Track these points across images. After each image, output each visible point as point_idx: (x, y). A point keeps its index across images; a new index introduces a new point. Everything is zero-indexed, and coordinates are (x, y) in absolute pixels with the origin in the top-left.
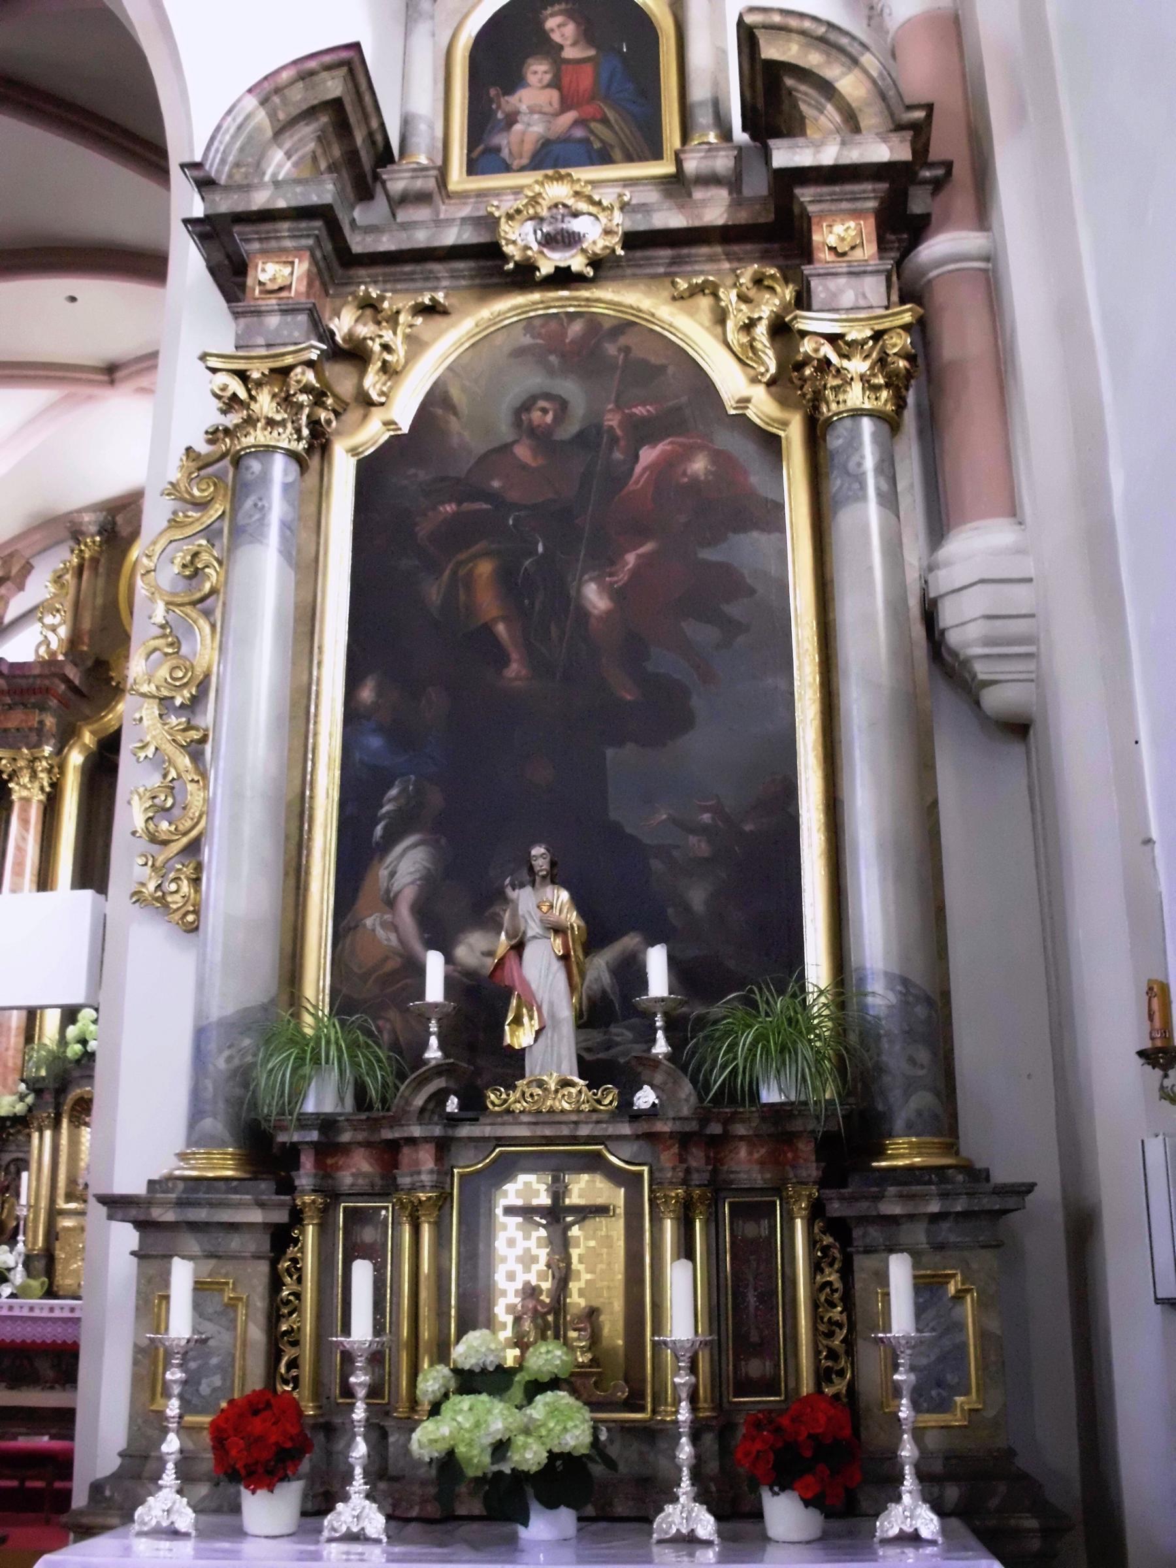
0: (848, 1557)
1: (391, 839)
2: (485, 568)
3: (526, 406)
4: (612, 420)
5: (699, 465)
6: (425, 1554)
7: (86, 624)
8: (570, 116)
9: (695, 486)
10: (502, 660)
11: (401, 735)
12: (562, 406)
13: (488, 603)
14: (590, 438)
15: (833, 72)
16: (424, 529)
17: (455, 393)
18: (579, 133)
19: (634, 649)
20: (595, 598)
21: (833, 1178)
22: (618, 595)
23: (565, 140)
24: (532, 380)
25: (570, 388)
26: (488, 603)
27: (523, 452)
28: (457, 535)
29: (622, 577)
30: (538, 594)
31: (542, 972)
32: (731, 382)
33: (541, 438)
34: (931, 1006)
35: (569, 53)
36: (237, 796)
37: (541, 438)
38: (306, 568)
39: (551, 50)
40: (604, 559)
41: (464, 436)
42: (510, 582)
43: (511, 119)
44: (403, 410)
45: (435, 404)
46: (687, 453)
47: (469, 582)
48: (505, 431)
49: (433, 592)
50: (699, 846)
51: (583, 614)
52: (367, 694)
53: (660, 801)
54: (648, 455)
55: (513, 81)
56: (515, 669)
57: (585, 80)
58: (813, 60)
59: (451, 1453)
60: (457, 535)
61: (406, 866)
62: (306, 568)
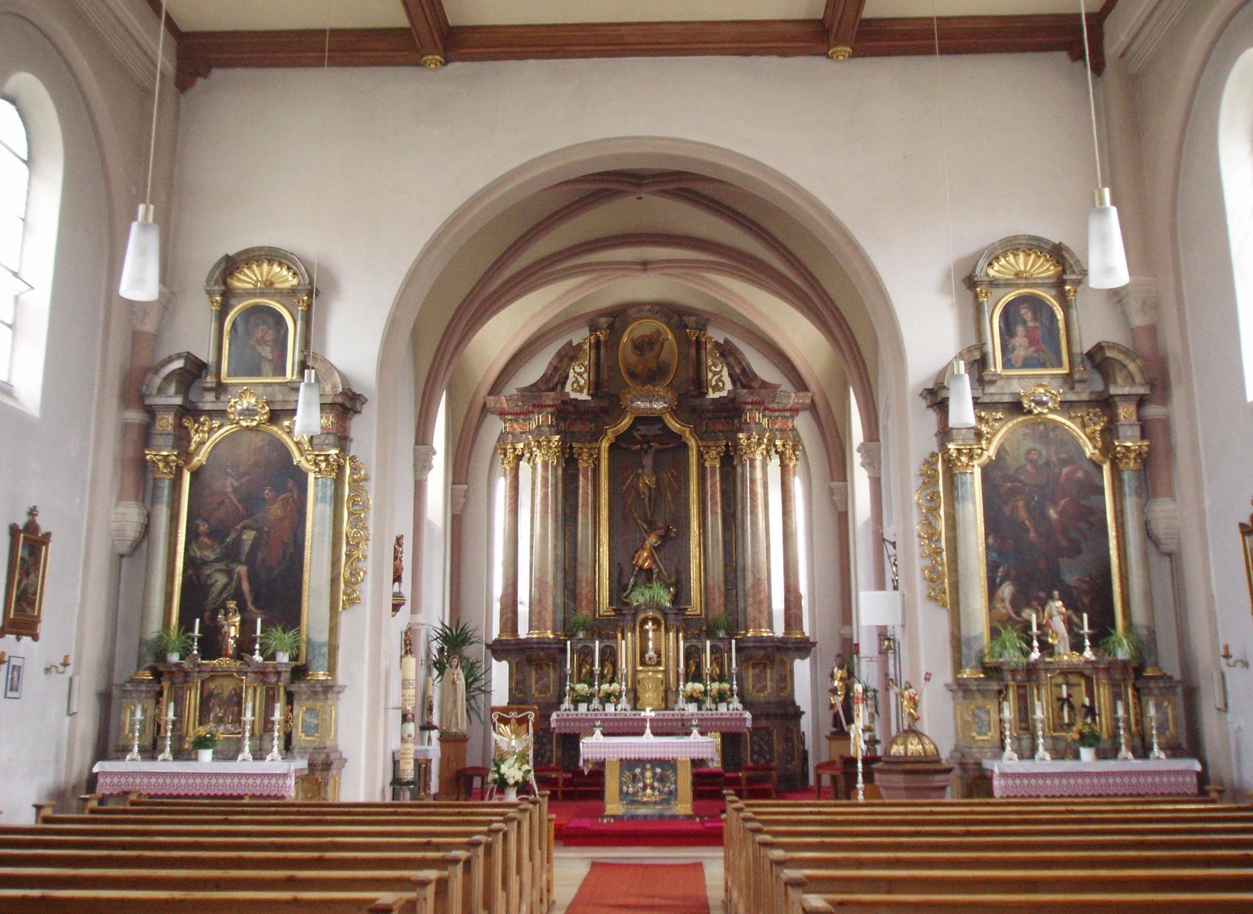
0: (791, 297)
1: (1000, 585)
2: (1021, 504)
3: (1029, 452)
4: (1054, 459)
5: (1080, 474)
6: (711, 262)
8: (1033, 348)
10: (1027, 531)
11: (1000, 552)
12: (1040, 454)
13: (1023, 514)
15: (1127, 362)
17: (1007, 447)
18: (1036, 355)
20: (1053, 514)
21: (1137, 678)
22: (1060, 513)
23: (1031, 358)
24: (1030, 444)
26: (1023, 514)
27: (1029, 468)
28: (1013, 492)
29: (1060, 508)
30: (1038, 513)
31: (1059, 625)
32: (1089, 450)
34: (1152, 632)
36: (905, 500)
39: (1024, 323)
40: (1054, 503)
41: (1011, 463)
42: (1029, 510)
43: (1014, 349)
44: (991, 452)
45: (1001, 451)
47: (1017, 507)
48: (1023, 461)
49: (1007, 510)
51: (1049, 520)
52: (991, 540)
54: (1065, 470)
56: (1032, 534)
58: (1121, 357)
60: (1013, 492)
62: (174, 519)
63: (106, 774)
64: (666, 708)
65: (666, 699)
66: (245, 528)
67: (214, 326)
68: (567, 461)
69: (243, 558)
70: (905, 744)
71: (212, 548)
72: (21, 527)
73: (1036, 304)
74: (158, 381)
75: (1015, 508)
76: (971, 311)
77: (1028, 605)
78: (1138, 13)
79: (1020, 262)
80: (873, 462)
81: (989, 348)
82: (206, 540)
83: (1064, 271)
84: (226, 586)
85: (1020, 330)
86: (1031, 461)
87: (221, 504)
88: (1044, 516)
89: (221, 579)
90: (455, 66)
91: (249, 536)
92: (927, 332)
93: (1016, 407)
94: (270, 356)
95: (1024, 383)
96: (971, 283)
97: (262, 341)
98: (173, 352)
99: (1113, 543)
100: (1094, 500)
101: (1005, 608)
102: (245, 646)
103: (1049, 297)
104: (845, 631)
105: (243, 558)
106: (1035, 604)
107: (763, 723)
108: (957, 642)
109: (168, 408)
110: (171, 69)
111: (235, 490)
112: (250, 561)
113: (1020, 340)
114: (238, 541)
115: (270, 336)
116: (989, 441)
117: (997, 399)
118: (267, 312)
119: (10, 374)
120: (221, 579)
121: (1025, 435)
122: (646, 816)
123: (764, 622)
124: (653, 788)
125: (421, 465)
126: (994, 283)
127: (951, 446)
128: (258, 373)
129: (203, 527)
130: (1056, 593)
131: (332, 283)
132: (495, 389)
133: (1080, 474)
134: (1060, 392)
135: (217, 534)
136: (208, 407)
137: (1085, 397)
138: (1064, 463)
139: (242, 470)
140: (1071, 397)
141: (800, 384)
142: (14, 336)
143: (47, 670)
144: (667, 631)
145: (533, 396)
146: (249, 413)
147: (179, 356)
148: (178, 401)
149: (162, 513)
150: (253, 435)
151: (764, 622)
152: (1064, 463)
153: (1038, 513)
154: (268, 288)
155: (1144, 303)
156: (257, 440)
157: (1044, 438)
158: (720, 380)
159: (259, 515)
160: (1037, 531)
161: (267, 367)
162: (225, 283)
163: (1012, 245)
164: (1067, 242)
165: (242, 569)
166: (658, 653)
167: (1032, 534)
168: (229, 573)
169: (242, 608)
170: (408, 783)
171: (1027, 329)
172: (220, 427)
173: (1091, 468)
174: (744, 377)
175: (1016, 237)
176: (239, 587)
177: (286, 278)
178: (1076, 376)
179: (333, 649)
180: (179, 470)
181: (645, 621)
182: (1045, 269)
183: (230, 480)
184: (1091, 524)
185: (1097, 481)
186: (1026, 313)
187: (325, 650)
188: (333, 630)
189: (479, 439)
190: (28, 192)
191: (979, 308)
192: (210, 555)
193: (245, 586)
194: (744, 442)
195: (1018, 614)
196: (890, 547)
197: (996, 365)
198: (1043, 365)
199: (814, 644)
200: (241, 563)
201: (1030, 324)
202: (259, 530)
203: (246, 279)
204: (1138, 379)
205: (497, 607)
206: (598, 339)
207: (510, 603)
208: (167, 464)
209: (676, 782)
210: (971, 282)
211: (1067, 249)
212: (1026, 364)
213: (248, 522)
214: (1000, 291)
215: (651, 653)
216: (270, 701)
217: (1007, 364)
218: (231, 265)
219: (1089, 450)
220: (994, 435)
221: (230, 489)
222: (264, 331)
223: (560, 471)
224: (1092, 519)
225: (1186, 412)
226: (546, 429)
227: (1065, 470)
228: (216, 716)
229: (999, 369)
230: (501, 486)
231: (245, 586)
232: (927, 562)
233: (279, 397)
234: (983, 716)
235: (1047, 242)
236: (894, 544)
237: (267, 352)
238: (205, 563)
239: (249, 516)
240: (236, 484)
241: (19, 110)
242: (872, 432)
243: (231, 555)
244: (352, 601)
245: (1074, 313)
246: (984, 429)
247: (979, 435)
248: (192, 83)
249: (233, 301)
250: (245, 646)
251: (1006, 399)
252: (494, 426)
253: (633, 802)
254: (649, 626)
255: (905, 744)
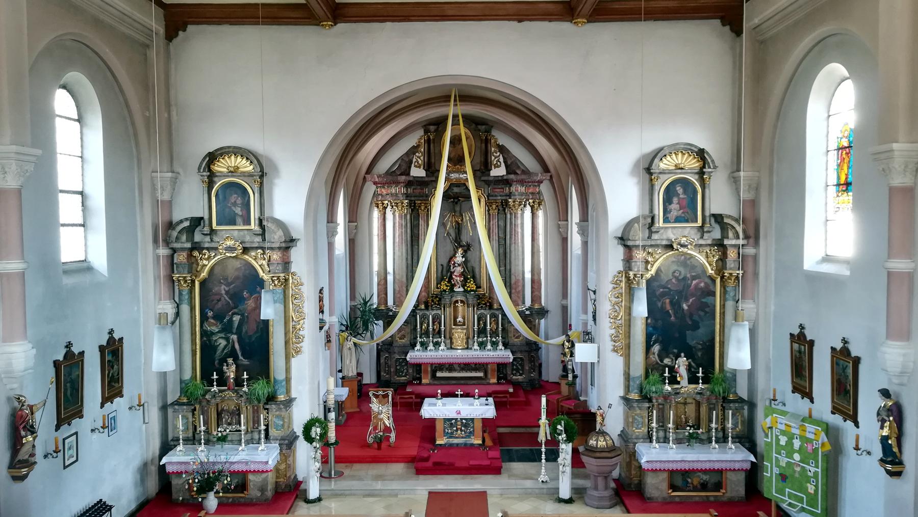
1: (654, 344)
2: (668, 301)
4: (688, 276)
5: (702, 285)
7: (397, 289)
9: (701, 288)
11: (654, 328)
13: (668, 307)
14: (685, 279)
15: (736, 225)
16: (658, 293)
19: (691, 315)
20: (685, 307)
22: (689, 306)
24: (675, 267)
25: (682, 269)
26: (668, 307)
27: (674, 281)
28: (663, 295)
30: (676, 305)
33: (676, 278)
35: (681, 196)
37: (676, 278)
38: (192, 309)
40: (687, 300)
44: (653, 272)
45: (658, 271)
46: (701, 282)
49: (659, 304)
50: (700, 347)
53: (694, 339)
54: (694, 282)
55: (671, 203)
56: (673, 318)
57: (685, 203)
58: (733, 223)
59: (547, 311)
61: (656, 348)
62: (192, 309)
63: (170, 463)
64: (467, 348)
65: (467, 343)
66: (233, 314)
67: (206, 196)
68: (412, 210)
69: (234, 331)
70: (597, 440)
71: (215, 325)
72: (105, 344)
73: (685, 183)
74: (175, 234)
75: (664, 303)
76: (647, 187)
77: (667, 357)
78: (768, 12)
79: (679, 159)
80: (583, 232)
81: (656, 212)
82: (212, 321)
83: (704, 167)
84: (225, 347)
85: (675, 200)
86: (675, 277)
87: (219, 300)
88: (680, 307)
89: (223, 343)
90: (341, 26)
91: (236, 319)
92: (622, 199)
93: (670, 247)
94: (240, 213)
95: (675, 231)
96: (647, 169)
97: (235, 204)
98: (182, 218)
99: (718, 326)
100: (708, 300)
101: (654, 358)
102: (239, 382)
103: (694, 179)
104: (564, 302)
105: (234, 331)
106: (671, 356)
107: (519, 355)
108: (627, 377)
109: (183, 249)
110: (162, 31)
111: (227, 293)
112: (239, 332)
113: (674, 206)
114: (231, 321)
115: (239, 201)
116: (652, 265)
117: (659, 242)
118: (236, 190)
119: (86, 257)
120: (223, 343)
121: (673, 262)
122: (457, 444)
123: (520, 303)
124: (461, 430)
125: (332, 233)
126: (663, 172)
127: (631, 274)
128: (234, 224)
129: (210, 314)
130: (683, 354)
131: (275, 169)
132: (369, 171)
133: (702, 285)
134: (695, 236)
135: (218, 317)
136: (206, 245)
137: (709, 242)
138: (694, 278)
139: (230, 280)
140: (702, 242)
141: (546, 169)
142: (85, 231)
143: (130, 408)
144: (468, 307)
145: (391, 177)
146: (231, 249)
147: (186, 219)
148: (189, 245)
149: (185, 308)
150: (234, 261)
151: (520, 303)
152: (694, 278)
153: (676, 305)
154: (234, 171)
155: (750, 186)
156: (237, 264)
157: (684, 264)
158: (498, 161)
159: (240, 307)
160: (675, 316)
161: (239, 220)
162: (210, 170)
163: (676, 149)
164: (707, 148)
165: (235, 337)
166: (464, 318)
167: (673, 318)
168: (227, 339)
169: (236, 359)
170: (332, 444)
171: (679, 199)
172: (214, 257)
173: (709, 281)
174: (512, 166)
175: (677, 144)
176: (233, 346)
177: (246, 166)
178: (705, 230)
179: (288, 380)
180: (193, 282)
181: (457, 302)
182: (692, 163)
183: (223, 287)
184: (706, 313)
185: (711, 288)
186: (679, 189)
187: (284, 383)
188: (288, 370)
189: (363, 195)
190: (82, 139)
191: (652, 187)
192: (215, 329)
193: (237, 346)
194: (511, 203)
195: (662, 361)
196: (592, 293)
197: (660, 223)
198: (687, 221)
199: (547, 311)
200: (233, 333)
201: (681, 196)
202: (242, 315)
203: (221, 167)
204: (741, 235)
205: (375, 280)
206: (429, 137)
207: (383, 282)
208: (186, 282)
209: (473, 427)
210: (648, 170)
211: (708, 153)
212: (677, 220)
213: (236, 310)
214: (666, 176)
215: (460, 319)
216: (256, 413)
217: (666, 220)
218: (212, 157)
219: (710, 271)
220: (655, 262)
221: (223, 292)
222: (235, 198)
223: (408, 216)
224: (707, 310)
225: (767, 252)
226: (400, 195)
227: (694, 282)
228: (226, 421)
229: (661, 224)
230: (376, 214)
231: (237, 346)
232: (613, 331)
233: (248, 238)
234: (640, 419)
235: (696, 147)
236: (595, 292)
237: (238, 210)
238: (213, 334)
239: (235, 308)
240: (227, 289)
241: (68, 91)
242: (584, 217)
243: (227, 329)
244: (298, 352)
245: (707, 191)
246: (650, 259)
247: (647, 262)
248: (177, 35)
249: (216, 179)
250: (239, 382)
251: (664, 243)
252: (370, 189)
253: (451, 437)
254: (459, 304)
255: (597, 440)
